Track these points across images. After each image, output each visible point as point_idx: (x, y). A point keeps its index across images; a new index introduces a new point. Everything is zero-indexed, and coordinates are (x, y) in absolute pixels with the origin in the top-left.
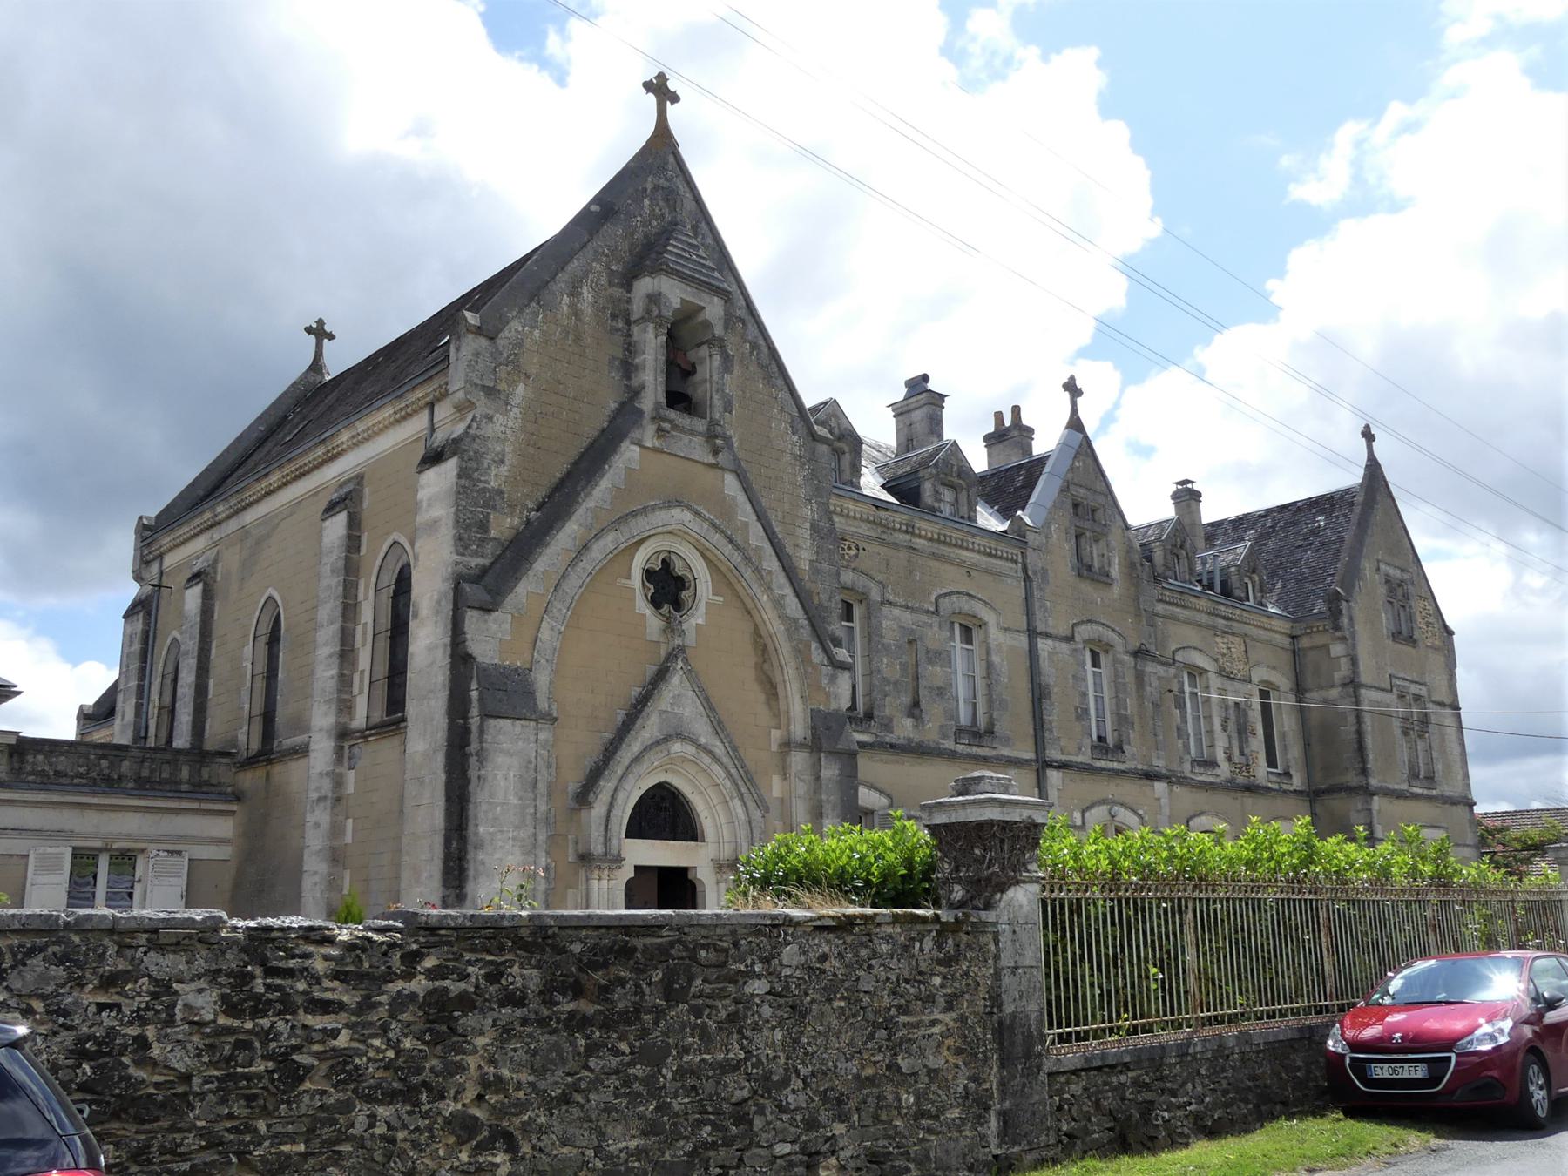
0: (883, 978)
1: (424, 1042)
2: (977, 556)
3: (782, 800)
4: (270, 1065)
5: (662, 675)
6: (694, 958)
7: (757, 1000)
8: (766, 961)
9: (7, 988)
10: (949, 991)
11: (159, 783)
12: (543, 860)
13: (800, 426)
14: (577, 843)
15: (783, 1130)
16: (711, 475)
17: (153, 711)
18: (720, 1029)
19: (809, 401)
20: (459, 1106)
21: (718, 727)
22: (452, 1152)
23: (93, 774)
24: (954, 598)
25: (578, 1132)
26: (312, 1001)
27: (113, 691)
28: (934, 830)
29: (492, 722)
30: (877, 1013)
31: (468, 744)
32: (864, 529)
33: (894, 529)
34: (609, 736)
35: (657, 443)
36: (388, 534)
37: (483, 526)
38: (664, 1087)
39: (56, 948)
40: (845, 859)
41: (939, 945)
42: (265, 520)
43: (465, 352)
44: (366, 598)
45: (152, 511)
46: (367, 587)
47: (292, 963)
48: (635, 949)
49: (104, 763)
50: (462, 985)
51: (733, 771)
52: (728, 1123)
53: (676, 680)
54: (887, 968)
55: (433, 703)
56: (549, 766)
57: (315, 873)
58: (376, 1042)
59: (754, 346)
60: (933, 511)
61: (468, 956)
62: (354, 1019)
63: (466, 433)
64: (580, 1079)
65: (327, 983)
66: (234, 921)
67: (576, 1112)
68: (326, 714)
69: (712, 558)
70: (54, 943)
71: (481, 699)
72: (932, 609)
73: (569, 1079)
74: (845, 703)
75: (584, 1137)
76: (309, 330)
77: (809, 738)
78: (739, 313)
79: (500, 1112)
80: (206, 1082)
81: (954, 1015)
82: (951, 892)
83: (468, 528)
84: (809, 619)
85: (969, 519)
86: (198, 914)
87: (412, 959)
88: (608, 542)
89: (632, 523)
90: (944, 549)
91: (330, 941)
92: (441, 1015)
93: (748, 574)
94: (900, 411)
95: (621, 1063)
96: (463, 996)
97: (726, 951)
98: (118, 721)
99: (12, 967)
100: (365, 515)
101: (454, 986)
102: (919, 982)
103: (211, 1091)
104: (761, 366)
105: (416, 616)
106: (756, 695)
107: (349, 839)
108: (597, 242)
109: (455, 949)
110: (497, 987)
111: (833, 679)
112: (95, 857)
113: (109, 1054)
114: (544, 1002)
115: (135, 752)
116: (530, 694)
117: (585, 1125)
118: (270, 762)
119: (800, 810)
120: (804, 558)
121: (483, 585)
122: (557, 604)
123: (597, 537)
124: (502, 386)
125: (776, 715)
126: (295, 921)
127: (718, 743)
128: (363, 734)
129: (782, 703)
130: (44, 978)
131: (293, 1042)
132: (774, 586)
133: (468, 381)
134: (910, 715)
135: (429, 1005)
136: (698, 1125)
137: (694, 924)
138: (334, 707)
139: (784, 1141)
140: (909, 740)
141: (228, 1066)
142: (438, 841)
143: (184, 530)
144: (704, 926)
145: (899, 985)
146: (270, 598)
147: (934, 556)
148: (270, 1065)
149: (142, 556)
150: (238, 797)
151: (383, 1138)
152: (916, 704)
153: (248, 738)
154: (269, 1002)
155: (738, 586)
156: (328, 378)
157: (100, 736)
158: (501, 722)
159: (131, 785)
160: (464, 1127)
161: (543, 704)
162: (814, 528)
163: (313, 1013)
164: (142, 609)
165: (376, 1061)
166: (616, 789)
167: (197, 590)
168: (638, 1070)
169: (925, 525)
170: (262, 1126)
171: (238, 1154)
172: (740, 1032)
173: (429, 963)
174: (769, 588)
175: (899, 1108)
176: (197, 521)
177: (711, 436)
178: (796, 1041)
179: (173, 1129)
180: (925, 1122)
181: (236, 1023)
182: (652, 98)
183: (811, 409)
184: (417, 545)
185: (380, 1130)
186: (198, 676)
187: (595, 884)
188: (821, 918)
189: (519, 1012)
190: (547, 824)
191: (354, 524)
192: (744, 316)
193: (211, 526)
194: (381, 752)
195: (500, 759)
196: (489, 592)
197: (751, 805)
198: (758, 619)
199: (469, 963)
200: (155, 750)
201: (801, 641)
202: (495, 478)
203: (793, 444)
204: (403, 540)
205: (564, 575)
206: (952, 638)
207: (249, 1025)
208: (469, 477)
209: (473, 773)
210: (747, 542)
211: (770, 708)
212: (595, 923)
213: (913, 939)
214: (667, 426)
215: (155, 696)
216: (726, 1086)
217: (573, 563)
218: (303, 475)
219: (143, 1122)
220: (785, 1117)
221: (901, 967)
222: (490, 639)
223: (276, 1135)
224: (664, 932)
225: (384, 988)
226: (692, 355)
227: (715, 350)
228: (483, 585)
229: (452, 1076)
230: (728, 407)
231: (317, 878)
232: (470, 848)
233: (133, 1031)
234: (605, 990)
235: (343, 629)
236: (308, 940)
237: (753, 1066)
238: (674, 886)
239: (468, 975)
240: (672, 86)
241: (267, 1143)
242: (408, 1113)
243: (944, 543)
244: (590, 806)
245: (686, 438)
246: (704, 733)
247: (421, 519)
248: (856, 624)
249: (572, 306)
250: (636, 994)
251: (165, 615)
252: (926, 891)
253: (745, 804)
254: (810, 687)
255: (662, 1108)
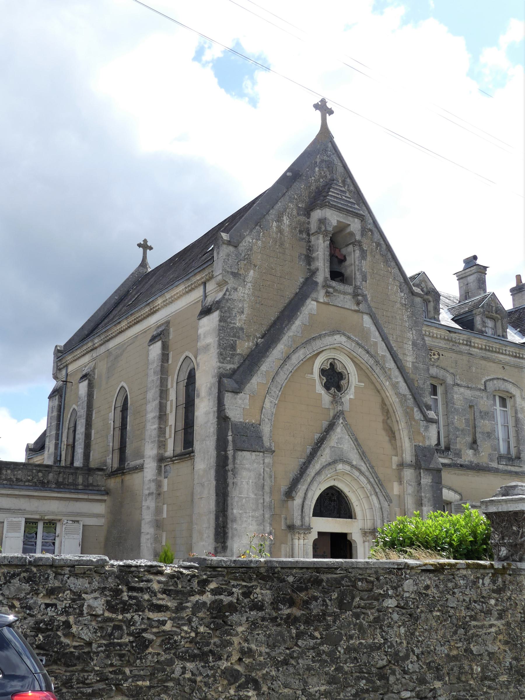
0: (461, 600)
1: (210, 629)
2: (508, 358)
3: (399, 496)
4: (131, 639)
5: (331, 427)
6: (354, 586)
7: (390, 610)
8: (395, 588)
9: (2, 594)
10: (499, 608)
11: (68, 485)
12: (268, 529)
13: (405, 287)
14: (286, 519)
15: (406, 684)
16: (356, 316)
17: (64, 447)
18: (370, 626)
19: (409, 273)
20: (229, 664)
21: (363, 455)
22: (226, 689)
23: (35, 480)
24: (495, 382)
25: (292, 681)
26: (152, 605)
27: (43, 436)
28: (488, 515)
29: (240, 453)
30: (458, 619)
31: (228, 465)
32: (442, 344)
33: (459, 343)
34: (303, 460)
35: (326, 300)
36: (183, 352)
37: (233, 347)
38: (339, 657)
39: (25, 574)
40: (438, 532)
41: (494, 582)
42: (119, 346)
43: (222, 255)
44: (172, 387)
45: (62, 343)
46: (172, 381)
47: (142, 585)
48: (322, 580)
49: (40, 474)
50: (230, 598)
51: (372, 480)
52: (375, 679)
53: (339, 430)
54: (464, 594)
55: (208, 443)
56: (271, 477)
57: (148, 533)
58: (185, 628)
59: (378, 245)
60: (481, 333)
61: (233, 583)
62: (174, 615)
63: (223, 298)
64: (294, 651)
65: (160, 596)
66: (112, 562)
67: (292, 670)
68: (152, 449)
69: (358, 362)
70: (24, 572)
71: (234, 441)
72: (483, 388)
73: (288, 651)
74: (434, 442)
75: (296, 684)
76: (139, 245)
77: (414, 461)
78: (369, 226)
79: (250, 668)
80: (99, 647)
81: (503, 622)
82: (500, 551)
83: (224, 349)
84: (413, 395)
85: (503, 336)
86: (94, 558)
87: (204, 583)
88: (301, 354)
89: (313, 344)
90: (489, 354)
91: (161, 573)
92: (219, 614)
93: (377, 370)
94: (461, 277)
95: (316, 643)
96: (231, 604)
97: (372, 582)
98: (46, 452)
99: (5, 584)
100: (171, 343)
101: (226, 599)
102: (483, 602)
103: (102, 651)
104: (383, 255)
105: (198, 396)
106: (384, 438)
107: (165, 515)
108: (291, 193)
109: (226, 578)
110: (248, 599)
111: (427, 428)
112: (36, 523)
113: (51, 630)
114: (274, 609)
115: (56, 469)
116: (259, 438)
117: (297, 677)
118: (123, 474)
119: (410, 502)
120: (409, 361)
121: (234, 378)
122: (273, 389)
123: (294, 352)
124: (242, 272)
125: (395, 448)
126: (143, 562)
127: (363, 464)
128: (172, 459)
129: (398, 442)
130: (19, 590)
131: (143, 626)
132: (392, 376)
133: (224, 270)
134: (471, 448)
135: (213, 609)
136: (358, 679)
137: (355, 567)
138: (156, 445)
139: (406, 690)
140: (471, 462)
141: (110, 639)
142: (212, 517)
143: (78, 352)
144: (360, 568)
145: (471, 604)
146: (122, 387)
147: (484, 358)
148: (131, 639)
149: (57, 366)
150: (107, 492)
151: (189, 680)
152: (475, 442)
153: (112, 461)
154: (130, 605)
155: (372, 377)
156: (149, 270)
157: (37, 460)
158: (245, 453)
159: (54, 486)
160: (232, 676)
161: (267, 444)
162: (414, 344)
163: (153, 611)
164: (58, 394)
165: (185, 638)
166: (307, 489)
167: (85, 383)
168: (325, 648)
169: (477, 341)
170: (127, 671)
171: (116, 685)
172: (381, 628)
173: (213, 586)
174: (389, 378)
175: (472, 674)
176: (85, 348)
177: (355, 295)
178: (413, 634)
179: (83, 670)
180: (487, 683)
181: (114, 616)
182: (318, 113)
183: (410, 278)
184: (198, 358)
185: (188, 675)
186: (87, 429)
187: (296, 542)
188: (425, 565)
189: (260, 614)
190: (270, 508)
191: (165, 347)
192: (372, 229)
193: (92, 350)
194: (180, 469)
195: (245, 473)
196: (237, 383)
197: (382, 498)
198: (384, 396)
199: (233, 586)
200: (66, 467)
201: (408, 407)
202: (239, 321)
203: (401, 298)
204: (191, 356)
205: (277, 373)
206: (495, 404)
207: (120, 617)
208: (225, 321)
209: (230, 481)
210: (376, 352)
211: (392, 445)
212: (300, 566)
213: (478, 578)
214: (331, 290)
215: (64, 439)
216: (373, 658)
217: (281, 367)
218: (138, 322)
219: (68, 666)
220: (407, 677)
221: (472, 594)
222: (238, 408)
223: (135, 676)
224: (338, 571)
225: (189, 598)
226: (344, 251)
227: (357, 248)
228: (234, 378)
229: (225, 647)
230: (364, 279)
231: (148, 536)
232: (229, 521)
233: (63, 618)
234: (306, 603)
235: (161, 404)
236: (149, 572)
237: (389, 647)
238: (340, 545)
239: (233, 593)
240: (329, 105)
241: (130, 680)
242: (202, 667)
243: (489, 350)
244: (293, 499)
245: (342, 296)
246: (355, 459)
247: (200, 344)
248: (439, 397)
249: (278, 227)
250: (323, 605)
251: (69, 396)
252: (485, 550)
253: (378, 498)
254: (413, 434)
255: (339, 669)
